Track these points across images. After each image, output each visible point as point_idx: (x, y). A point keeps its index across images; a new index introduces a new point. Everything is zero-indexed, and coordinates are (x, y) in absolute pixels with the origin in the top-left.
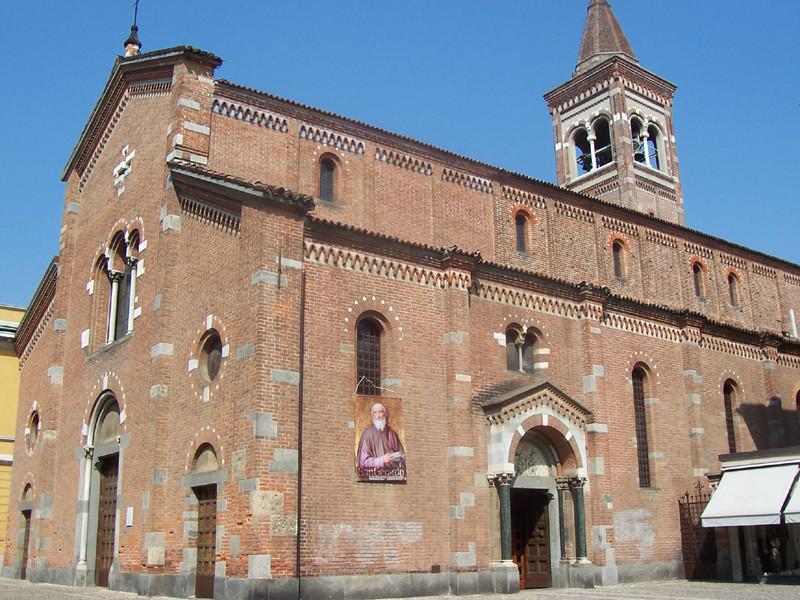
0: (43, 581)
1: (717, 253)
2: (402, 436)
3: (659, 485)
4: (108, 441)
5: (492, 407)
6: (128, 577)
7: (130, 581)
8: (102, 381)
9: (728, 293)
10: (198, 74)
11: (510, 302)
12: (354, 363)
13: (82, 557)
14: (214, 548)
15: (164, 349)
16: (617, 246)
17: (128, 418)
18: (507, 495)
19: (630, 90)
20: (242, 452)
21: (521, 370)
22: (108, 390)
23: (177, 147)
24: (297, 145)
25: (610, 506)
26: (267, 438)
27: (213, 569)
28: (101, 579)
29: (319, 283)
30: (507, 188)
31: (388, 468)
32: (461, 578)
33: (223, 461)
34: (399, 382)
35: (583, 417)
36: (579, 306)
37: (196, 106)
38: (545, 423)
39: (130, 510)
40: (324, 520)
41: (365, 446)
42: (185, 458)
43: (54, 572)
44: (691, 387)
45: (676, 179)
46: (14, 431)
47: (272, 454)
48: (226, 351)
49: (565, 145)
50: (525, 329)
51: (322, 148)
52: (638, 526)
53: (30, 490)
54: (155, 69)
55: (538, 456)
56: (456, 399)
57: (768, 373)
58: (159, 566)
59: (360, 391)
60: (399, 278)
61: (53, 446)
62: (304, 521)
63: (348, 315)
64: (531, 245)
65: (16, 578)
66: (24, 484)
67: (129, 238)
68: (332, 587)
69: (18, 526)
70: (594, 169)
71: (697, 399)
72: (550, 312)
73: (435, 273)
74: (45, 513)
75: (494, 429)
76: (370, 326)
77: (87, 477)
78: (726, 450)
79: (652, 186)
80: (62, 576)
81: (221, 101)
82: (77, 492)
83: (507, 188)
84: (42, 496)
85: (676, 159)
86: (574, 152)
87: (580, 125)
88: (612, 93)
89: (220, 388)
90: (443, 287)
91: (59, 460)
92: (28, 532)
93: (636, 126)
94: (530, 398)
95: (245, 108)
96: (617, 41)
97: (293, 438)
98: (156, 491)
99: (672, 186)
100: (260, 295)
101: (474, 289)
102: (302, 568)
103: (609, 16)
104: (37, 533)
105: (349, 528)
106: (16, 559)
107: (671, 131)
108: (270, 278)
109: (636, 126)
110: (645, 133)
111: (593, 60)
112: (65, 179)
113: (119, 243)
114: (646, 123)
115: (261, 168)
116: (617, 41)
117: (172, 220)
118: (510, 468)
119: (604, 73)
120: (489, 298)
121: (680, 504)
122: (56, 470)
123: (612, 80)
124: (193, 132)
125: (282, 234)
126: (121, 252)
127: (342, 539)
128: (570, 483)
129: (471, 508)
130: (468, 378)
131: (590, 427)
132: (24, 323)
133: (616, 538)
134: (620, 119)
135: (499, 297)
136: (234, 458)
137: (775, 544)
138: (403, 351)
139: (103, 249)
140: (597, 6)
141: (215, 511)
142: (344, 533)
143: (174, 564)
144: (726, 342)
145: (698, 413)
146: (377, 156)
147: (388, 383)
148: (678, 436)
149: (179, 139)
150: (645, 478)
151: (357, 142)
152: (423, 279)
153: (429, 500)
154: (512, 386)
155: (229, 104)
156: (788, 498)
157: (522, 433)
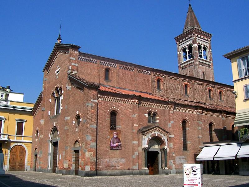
2: (121, 139)
4: (55, 138)
5: (143, 132)
6: (60, 171)
7: (60, 172)
8: (53, 124)
9: (219, 97)
10: (75, 51)
11: (149, 106)
13: (50, 166)
15: (68, 118)
16: (186, 86)
18: (146, 152)
19: (198, 37)
21: (152, 122)
22: (55, 126)
24: (99, 67)
25: (174, 155)
28: (54, 171)
30: (155, 73)
31: (117, 146)
32: (134, 171)
34: (120, 127)
35: (166, 134)
36: (167, 106)
37: (74, 59)
38: (157, 135)
39: (60, 155)
40: (102, 158)
41: (112, 142)
43: (43, 170)
44: (199, 125)
45: (211, 62)
46: (32, 134)
48: (81, 120)
49: (180, 52)
51: (105, 67)
52: (182, 160)
54: (64, 48)
55: (156, 143)
56: (134, 130)
57: (223, 120)
59: (111, 129)
60: (121, 102)
61: (42, 139)
62: (98, 158)
64: (161, 87)
66: (35, 148)
68: (104, 173)
69: (33, 158)
70: (188, 60)
71: (200, 128)
72: (160, 108)
76: (113, 114)
77: (50, 146)
78: (209, 141)
79: (204, 64)
80: (45, 171)
81: (80, 57)
82: (48, 151)
83: (155, 73)
84: (40, 151)
85: (212, 56)
86: (182, 54)
88: (193, 38)
91: (44, 142)
92: (36, 160)
93: (200, 47)
94: (153, 130)
95: (86, 58)
96: (195, 22)
97: (95, 140)
98: (66, 151)
99: (210, 64)
101: (140, 104)
102: (97, 169)
103: (193, 15)
104: (38, 160)
105: (108, 160)
106: (33, 166)
107: (210, 48)
108: (90, 105)
111: (188, 28)
112: (44, 72)
114: (203, 46)
116: (195, 22)
117: (69, 87)
118: (147, 146)
119: (190, 33)
120: (144, 106)
122: (43, 145)
123: (193, 35)
126: (58, 92)
127: (106, 162)
128: (163, 150)
130: (137, 125)
132: (34, 108)
134: (195, 45)
135: (145, 105)
136: (82, 145)
137: (216, 165)
138: (121, 120)
139: (53, 91)
140: (190, 12)
142: (107, 161)
144: (210, 113)
145: (201, 132)
146: (120, 68)
147: (118, 127)
148: (195, 138)
149: (70, 67)
150: (185, 148)
151: (115, 64)
152: (127, 102)
154: (149, 126)
155: (82, 58)
156: (237, 153)
157: (150, 138)
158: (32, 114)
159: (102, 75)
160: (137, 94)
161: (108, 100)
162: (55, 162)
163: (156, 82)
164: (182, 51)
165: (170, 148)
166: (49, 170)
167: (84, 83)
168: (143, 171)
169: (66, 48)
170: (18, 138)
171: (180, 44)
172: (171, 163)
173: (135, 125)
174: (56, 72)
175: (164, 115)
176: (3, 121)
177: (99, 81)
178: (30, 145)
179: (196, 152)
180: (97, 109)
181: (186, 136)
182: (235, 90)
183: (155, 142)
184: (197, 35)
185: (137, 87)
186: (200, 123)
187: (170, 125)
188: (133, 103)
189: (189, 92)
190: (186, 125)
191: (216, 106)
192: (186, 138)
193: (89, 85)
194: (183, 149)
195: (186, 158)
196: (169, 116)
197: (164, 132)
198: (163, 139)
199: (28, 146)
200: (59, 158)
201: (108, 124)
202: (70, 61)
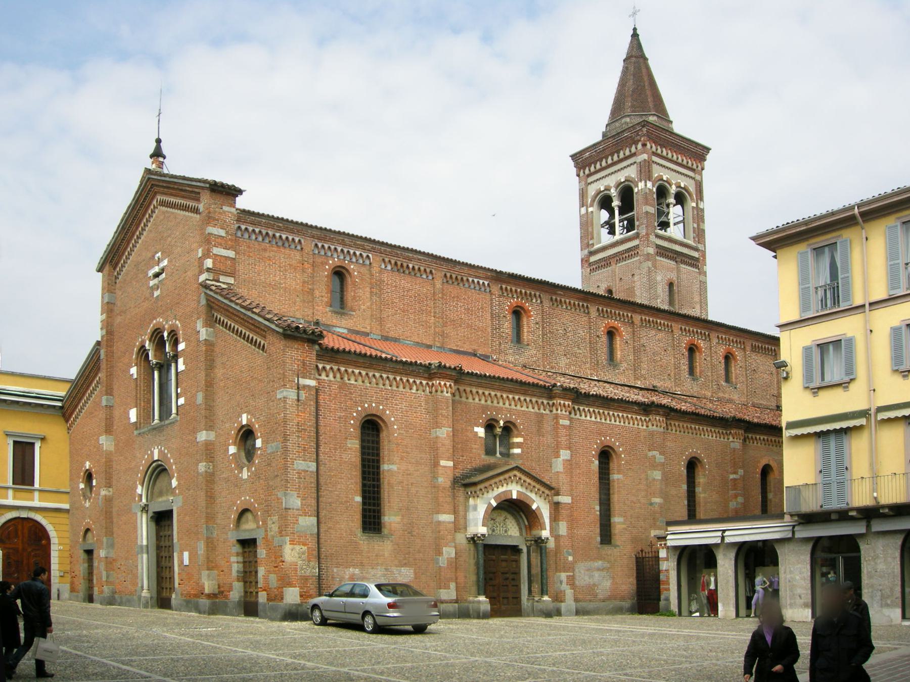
0: (111, 604)
1: (714, 335)
3: (618, 543)
5: (467, 483)
7: (191, 604)
8: (152, 453)
12: (359, 454)
14: (257, 582)
17: (179, 484)
18: (481, 549)
20: (275, 518)
21: (498, 455)
23: (208, 270)
27: (257, 596)
28: (163, 602)
29: (330, 395)
34: (394, 467)
35: (547, 492)
37: (222, 233)
38: (514, 497)
39: (186, 555)
40: (338, 565)
42: (230, 518)
44: (654, 466)
48: (259, 443)
49: (590, 209)
50: (502, 423)
51: (334, 261)
52: (596, 574)
53: (89, 534)
56: (440, 480)
63: (353, 418)
64: (525, 336)
66: (83, 529)
70: (618, 237)
71: (657, 475)
72: (524, 408)
73: (424, 382)
74: (108, 553)
75: (471, 501)
76: (371, 427)
78: (683, 513)
87: (606, 190)
89: (256, 470)
90: (431, 392)
93: (662, 192)
94: (502, 478)
105: (357, 571)
106: (81, 585)
108: (292, 394)
111: (623, 120)
114: (673, 190)
115: (280, 284)
121: (637, 558)
122: (115, 520)
123: (640, 146)
128: (536, 541)
130: (451, 464)
131: (556, 499)
133: (577, 583)
135: (478, 399)
136: (270, 522)
143: (225, 593)
149: (209, 263)
150: (606, 536)
152: (415, 388)
153: (419, 552)
154: (488, 468)
157: (494, 504)
158: (64, 415)
159: (322, 290)
160: (451, 361)
161: (353, 379)
162: (166, 574)
163: (509, 317)
165: (557, 537)
167: (267, 323)
168: (471, 606)
169: (185, 191)
170: (19, 494)
171: (590, 179)
172: (561, 582)
173: (443, 463)
174: (151, 273)
175: (540, 432)
177: (310, 312)
178: (63, 519)
179: (642, 551)
180: (317, 409)
181: (609, 500)
182: (784, 355)
183: (509, 516)
184: (654, 149)
185: (443, 335)
186: (657, 460)
187: (558, 465)
188: (434, 391)
189: (619, 353)
190: (611, 464)
191: (711, 401)
192: (609, 505)
193: (284, 330)
194: (599, 539)
195: (608, 569)
196: (557, 436)
197: (538, 486)
198: (534, 507)
199: (56, 521)
201: (353, 460)
202: (208, 241)
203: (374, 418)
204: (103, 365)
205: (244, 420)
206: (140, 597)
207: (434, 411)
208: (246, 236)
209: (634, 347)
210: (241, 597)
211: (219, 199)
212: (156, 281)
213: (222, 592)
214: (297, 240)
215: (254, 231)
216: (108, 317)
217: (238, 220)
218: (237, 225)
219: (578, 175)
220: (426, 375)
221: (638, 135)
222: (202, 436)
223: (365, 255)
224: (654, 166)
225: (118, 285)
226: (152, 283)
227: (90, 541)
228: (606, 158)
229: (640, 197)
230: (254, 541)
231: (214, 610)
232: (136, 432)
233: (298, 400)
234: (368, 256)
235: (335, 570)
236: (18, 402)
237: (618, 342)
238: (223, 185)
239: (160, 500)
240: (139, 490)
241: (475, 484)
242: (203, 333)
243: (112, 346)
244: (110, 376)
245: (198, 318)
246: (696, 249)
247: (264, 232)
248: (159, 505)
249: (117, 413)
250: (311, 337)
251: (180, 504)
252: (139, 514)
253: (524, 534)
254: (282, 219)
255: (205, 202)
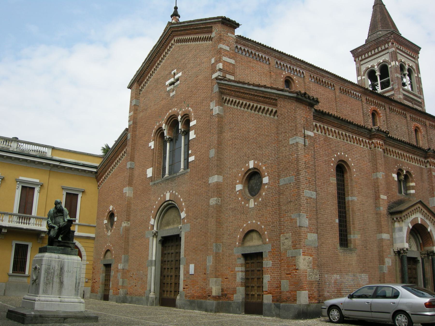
0: (124, 302)
5: (396, 212)
7: (197, 302)
8: (165, 196)
13: (152, 290)
23: (220, 70)
26: (304, 227)
33: (267, 240)
34: (355, 199)
37: (228, 48)
38: (420, 222)
39: (192, 267)
42: (236, 237)
47: (307, 236)
49: (363, 77)
50: (405, 172)
51: (286, 73)
53: (109, 253)
58: (218, 296)
63: (333, 162)
65: (101, 300)
67: (181, 119)
75: (397, 225)
76: (341, 169)
87: (371, 67)
89: (263, 200)
90: (370, 148)
93: (402, 67)
100: (297, 150)
105: (338, 277)
106: (100, 289)
108: (300, 140)
109: (402, 67)
110: (407, 72)
111: (378, 33)
113: (173, 122)
114: (407, 67)
122: (130, 243)
123: (390, 44)
124: (227, 62)
125: (304, 117)
127: (335, 282)
129: (390, 266)
132: (102, 164)
141: (262, 267)
149: (220, 66)
158: (96, 178)
164: (366, 74)
166: (150, 300)
171: (362, 63)
174: (167, 83)
176: (37, 190)
178: (91, 244)
189: (421, 142)
198: (429, 230)
200: (187, 271)
203: (343, 163)
204: (129, 143)
205: (251, 165)
206: (148, 298)
207: (374, 160)
208: (240, 52)
209: (428, 139)
210: (243, 298)
211: (226, 29)
212: (172, 87)
213: (226, 295)
214: (267, 58)
215: (244, 49)
216: (135, 113)
217: (236, 42)
218: (235, 45)
219: (355, 61)
220: (368, 136)
221: (389, 38)
222: (214, 179)
223: (301, 71)
224: (398, 55)
225: (141, 95)
226: (168, 89)
227: (109, 258)
228: (371, 51)
229: (393, 70)
230: (260, 255)
231: (219, 309)
232: (151, 184)
233: (305, 145)
234: (303, 72)
235: (326, 276)
236: (71, 168)
237: (420, 136)
238: (229, 20)
239: (167, 228)
240: (152, 222)
241: (401, 212)
242: (216, 110)
243: (135, 131)
244: (133, 149)
245: (211, 101)
246: (420, 98)
247: (250, 51)
248: (169, 231)
249: (136, 173)
250: (312, 102)
251: (188, 230)
252: (151, 238)
253: (420, 250)
254: (260, 44)
255: (217, 31)
